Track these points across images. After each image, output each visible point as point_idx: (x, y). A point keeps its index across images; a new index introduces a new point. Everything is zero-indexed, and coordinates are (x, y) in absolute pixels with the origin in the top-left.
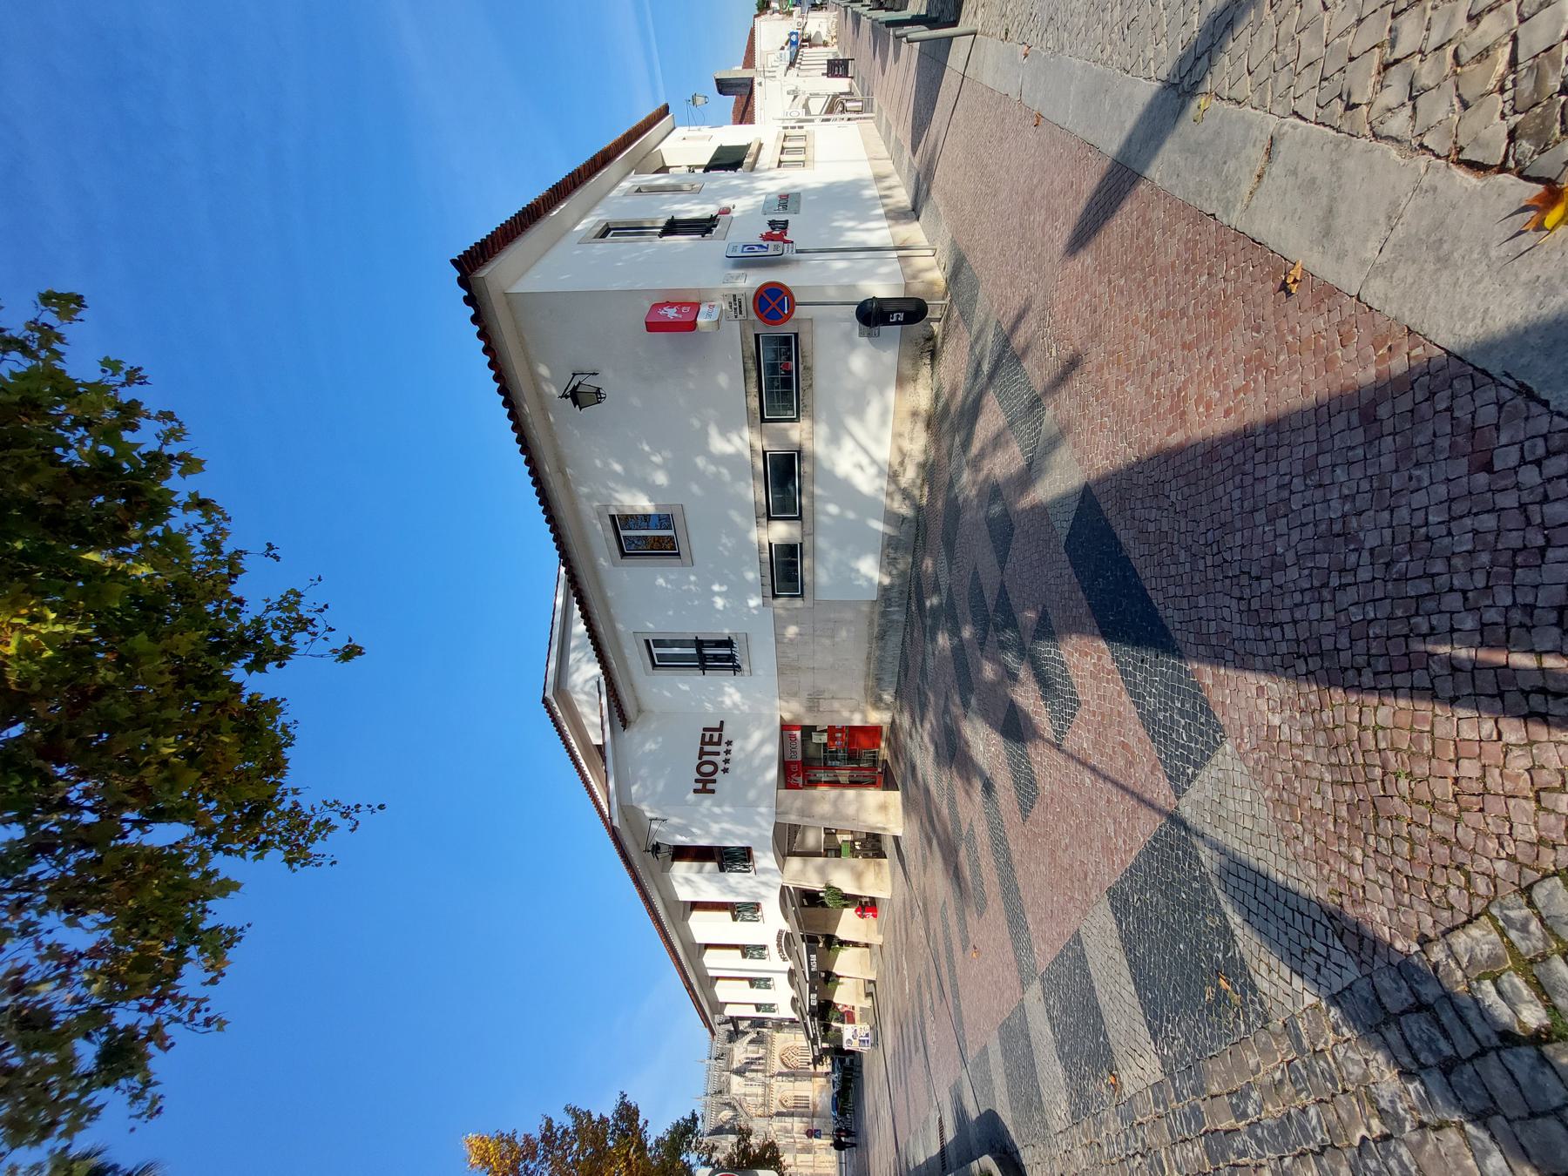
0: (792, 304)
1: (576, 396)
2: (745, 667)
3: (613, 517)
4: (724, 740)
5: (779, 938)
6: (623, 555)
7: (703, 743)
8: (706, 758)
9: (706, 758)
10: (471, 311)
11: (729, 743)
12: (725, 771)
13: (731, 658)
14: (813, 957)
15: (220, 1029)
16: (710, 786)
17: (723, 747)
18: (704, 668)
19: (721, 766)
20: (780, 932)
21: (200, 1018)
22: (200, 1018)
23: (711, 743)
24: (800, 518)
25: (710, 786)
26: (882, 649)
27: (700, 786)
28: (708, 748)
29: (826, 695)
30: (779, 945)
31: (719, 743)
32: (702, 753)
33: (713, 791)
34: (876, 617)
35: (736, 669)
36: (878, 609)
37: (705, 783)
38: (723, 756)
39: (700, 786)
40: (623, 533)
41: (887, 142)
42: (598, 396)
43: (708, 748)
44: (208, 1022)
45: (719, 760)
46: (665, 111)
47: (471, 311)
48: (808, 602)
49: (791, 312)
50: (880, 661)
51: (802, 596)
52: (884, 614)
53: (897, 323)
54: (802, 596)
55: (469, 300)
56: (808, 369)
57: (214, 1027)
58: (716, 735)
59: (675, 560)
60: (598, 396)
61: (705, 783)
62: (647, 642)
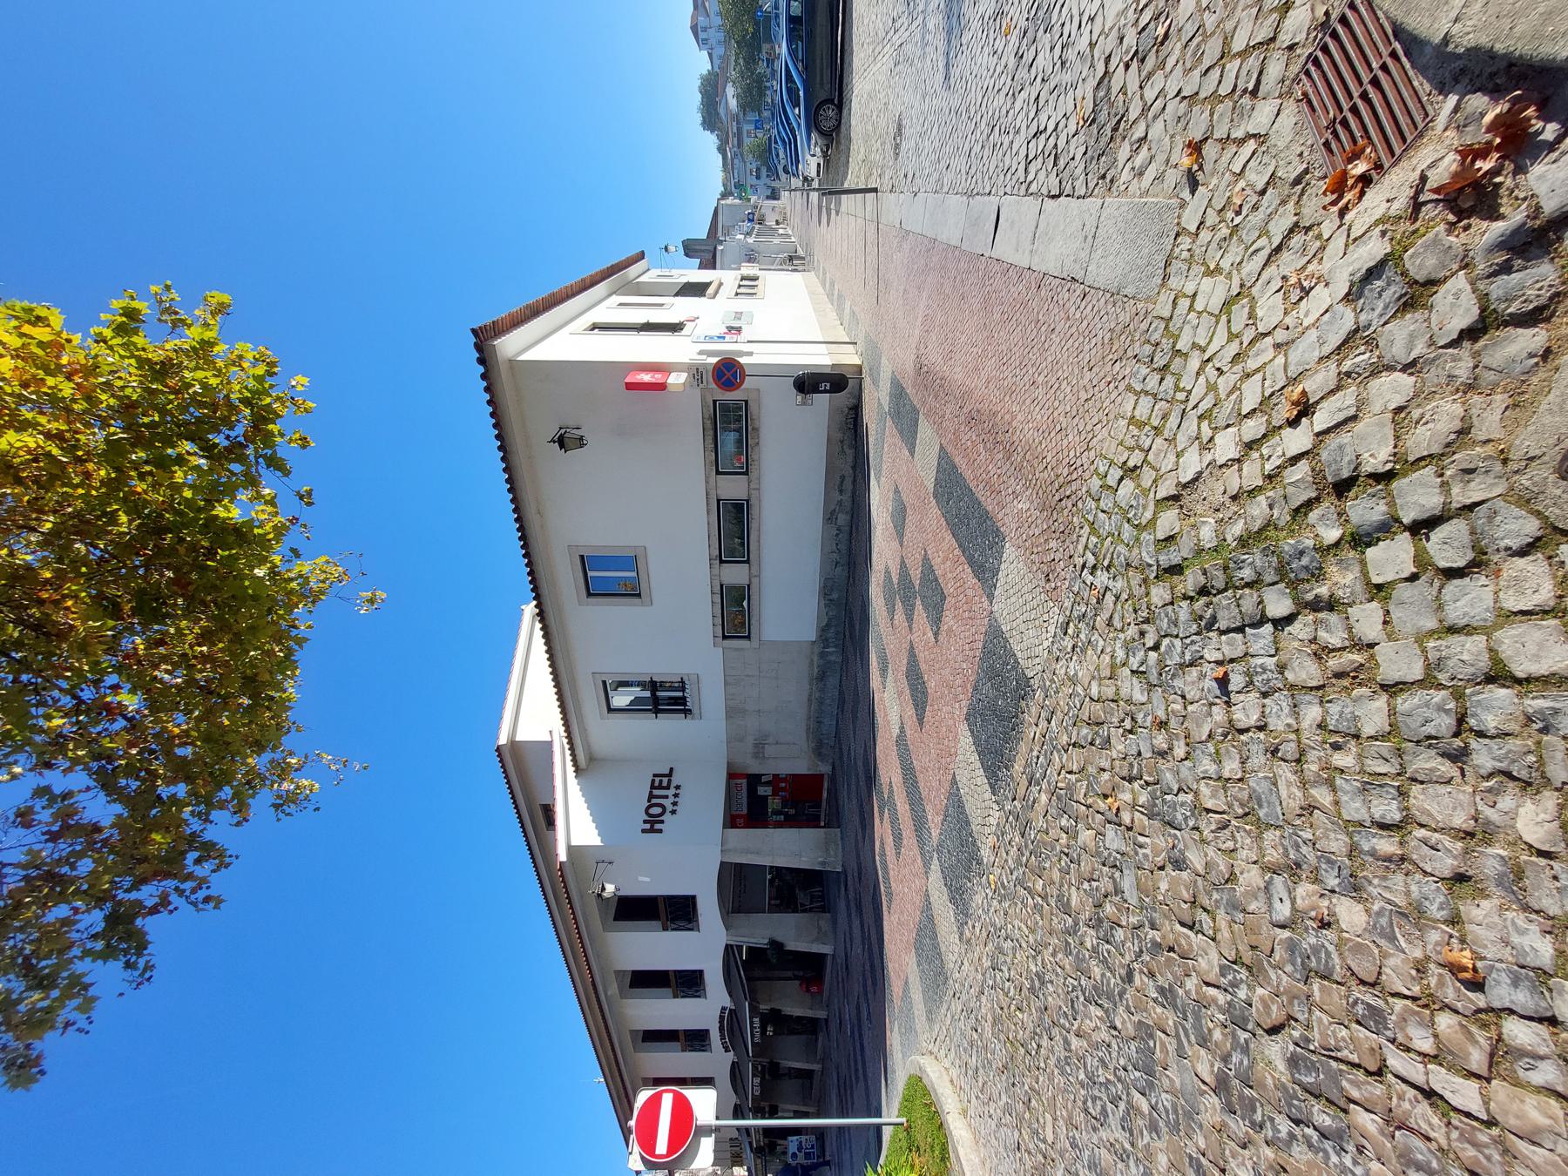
0: (743, 376)
1: (561, 442)
2: (695, 711)
3: (582, 557)
4: (673, 784)
5: (721, 1018)
6: (589, 594)
7: (653, 787)
8: (654, 801)
9: (654, 801)
10: (481, 369)
11: (678, 787)
12: (673, 812)
13: (682, 701)
14: (756, 1020)
15: (274, 805)
16: (657, 826)
17: (672, 791)
18: (657, 711)
19: (670, 808)
20: (724, 1009)
21: (201, 894)
22: (201, 894)
23: (660, 787)
24: (748, 562)
25: (657, 826)
26: (822, 690)
27: (648, 826)
28: (656, 792)
29: (771, 740)
30: (721, 1029)
31: (668, 788)
32: (651, 796)
33: (660, 831)
34: (816, 658)
35: (687, 712)
36: (817, 650)
37: (652, 823)
38: (672, 799)
39: (648, 826)
40: (590, 574)
41: (824, 286)
42: (580, 442)
43: (656, 792)
44: (207, 900)
45: (667, 803)
46: (641, 256)
47: (481, 369)
48: (754, 642)
49: (742, 381)
50: (821, 702)
51: (748, 637)
52: (822, 655)
53: (825, 391)
54: (748, 637)
55: (481, 361)
56: (756, 430)
57: (212, 904)
58: (665, 780)
59: (637, 600)
60: (580, 442)
61: (652, 823)
62: (604, 683)
